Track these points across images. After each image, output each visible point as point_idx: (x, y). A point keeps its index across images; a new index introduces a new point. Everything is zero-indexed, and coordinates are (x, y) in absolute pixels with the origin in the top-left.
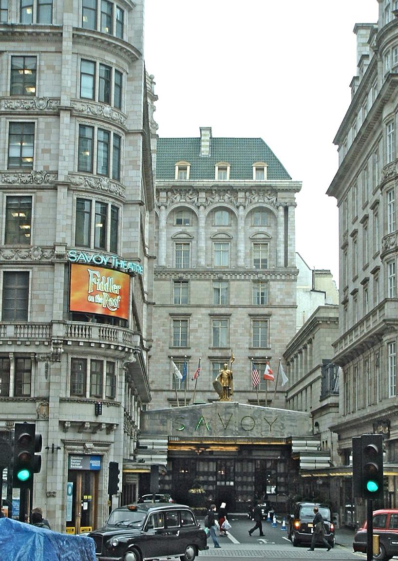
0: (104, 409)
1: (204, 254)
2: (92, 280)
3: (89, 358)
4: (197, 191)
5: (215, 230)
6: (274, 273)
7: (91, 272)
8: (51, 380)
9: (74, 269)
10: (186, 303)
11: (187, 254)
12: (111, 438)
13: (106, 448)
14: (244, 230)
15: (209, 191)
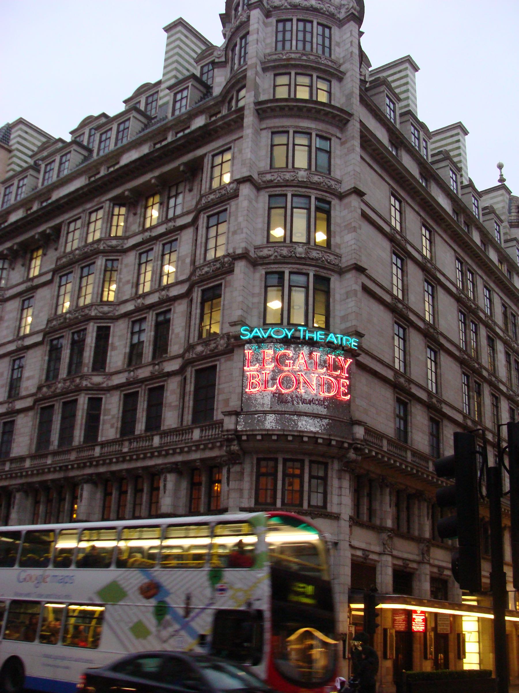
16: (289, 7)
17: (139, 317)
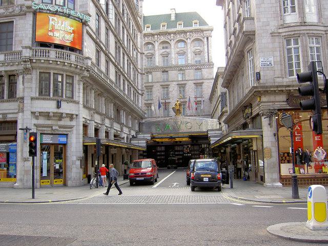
0: (64, 104)
1: (175, 60)
2: (51, 22)
3: (52, 72)
4: (170, 34)
5: (178, 50)
6: (203, 65)
7: (51, 18)
8: (27, 87)
9: (39, 17)
10: (168, 81)
11: (167, 60)
12: (73, 123)
13: (70, 130)
14: (191, 48)
15: (175, 33)
17: (249, 66)
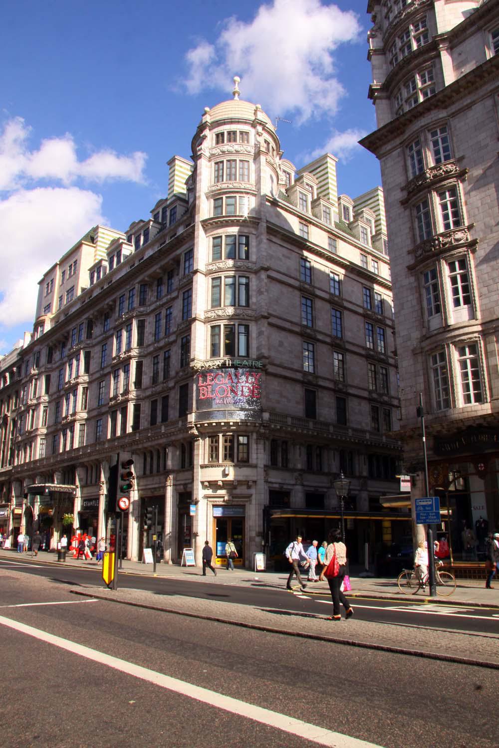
16: (221, 153)
